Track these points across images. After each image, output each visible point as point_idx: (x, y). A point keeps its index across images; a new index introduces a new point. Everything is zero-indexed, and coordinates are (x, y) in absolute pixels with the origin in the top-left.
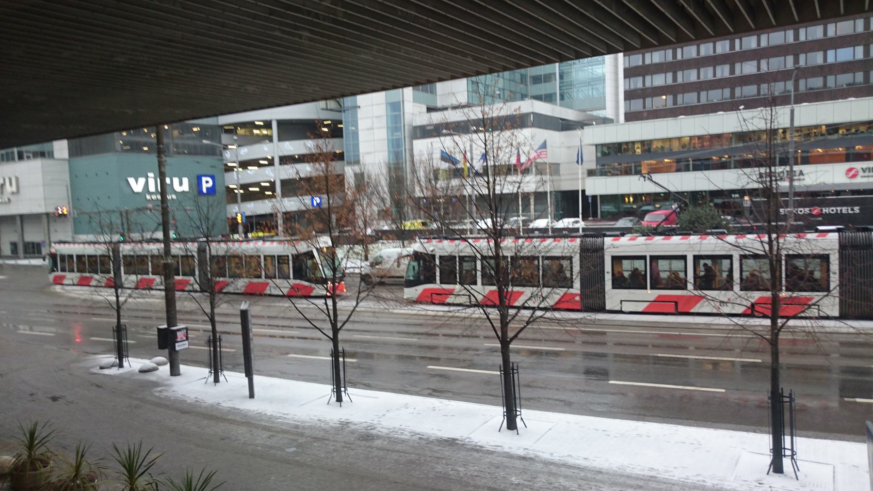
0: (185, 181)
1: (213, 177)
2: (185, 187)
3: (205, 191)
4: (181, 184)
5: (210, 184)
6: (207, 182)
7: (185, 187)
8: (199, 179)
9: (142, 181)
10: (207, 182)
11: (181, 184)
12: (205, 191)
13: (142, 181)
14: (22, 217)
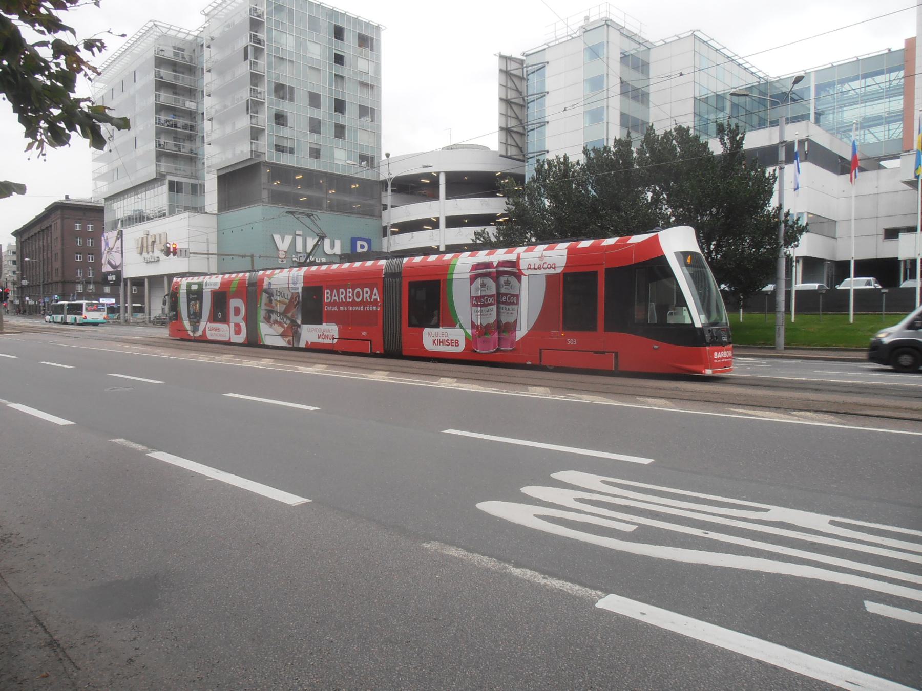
0: (338, 243)
1: (369, 241)
4: (333, 246)
5: (365, 249)
6: (362, 247)
8: (354, 241)
9: (288, 239)
10: (362, 247)
11: (333, 246)
13: (288, 239)
14: (150, 278)
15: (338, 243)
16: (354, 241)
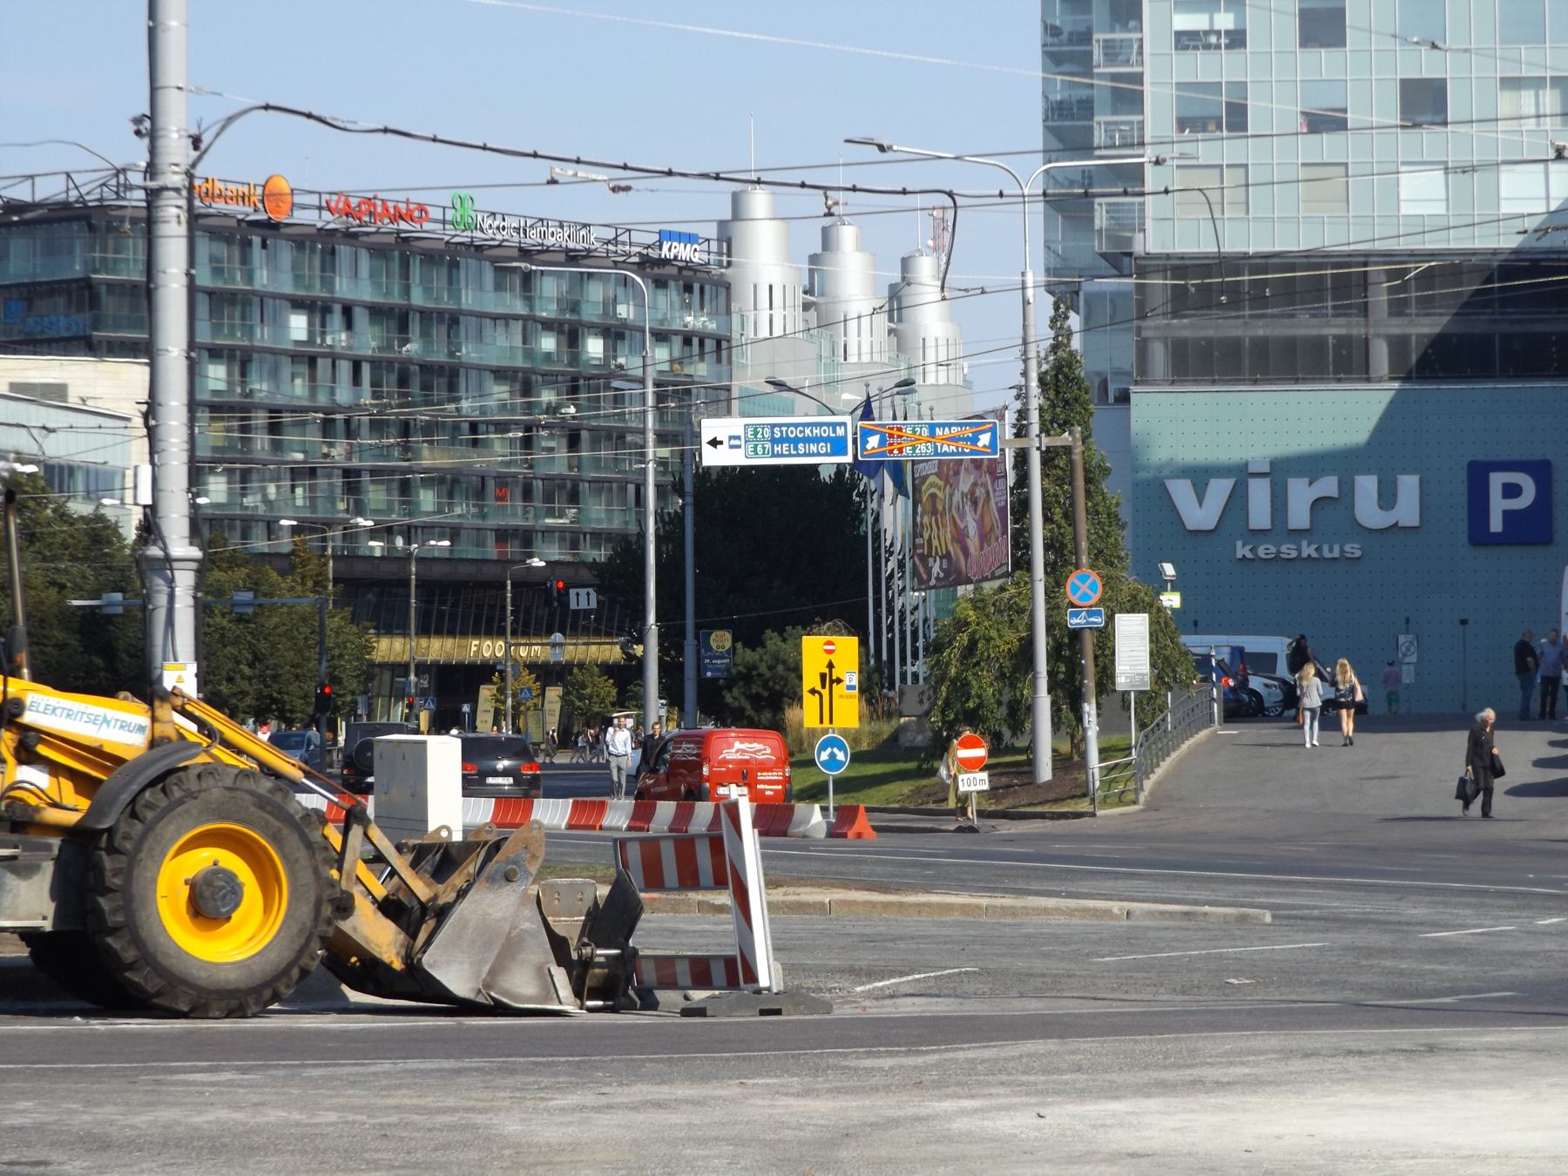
0: (1409, 485)
2: (1407, 511)
3: (1496, 525)
7: (1407, 511)
8: (1478, 475)
11: (1387, 498)
12: (1496, 525)
15: (1409, 485)
16: (1478, 475)
